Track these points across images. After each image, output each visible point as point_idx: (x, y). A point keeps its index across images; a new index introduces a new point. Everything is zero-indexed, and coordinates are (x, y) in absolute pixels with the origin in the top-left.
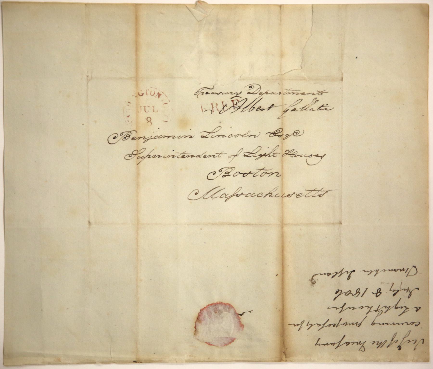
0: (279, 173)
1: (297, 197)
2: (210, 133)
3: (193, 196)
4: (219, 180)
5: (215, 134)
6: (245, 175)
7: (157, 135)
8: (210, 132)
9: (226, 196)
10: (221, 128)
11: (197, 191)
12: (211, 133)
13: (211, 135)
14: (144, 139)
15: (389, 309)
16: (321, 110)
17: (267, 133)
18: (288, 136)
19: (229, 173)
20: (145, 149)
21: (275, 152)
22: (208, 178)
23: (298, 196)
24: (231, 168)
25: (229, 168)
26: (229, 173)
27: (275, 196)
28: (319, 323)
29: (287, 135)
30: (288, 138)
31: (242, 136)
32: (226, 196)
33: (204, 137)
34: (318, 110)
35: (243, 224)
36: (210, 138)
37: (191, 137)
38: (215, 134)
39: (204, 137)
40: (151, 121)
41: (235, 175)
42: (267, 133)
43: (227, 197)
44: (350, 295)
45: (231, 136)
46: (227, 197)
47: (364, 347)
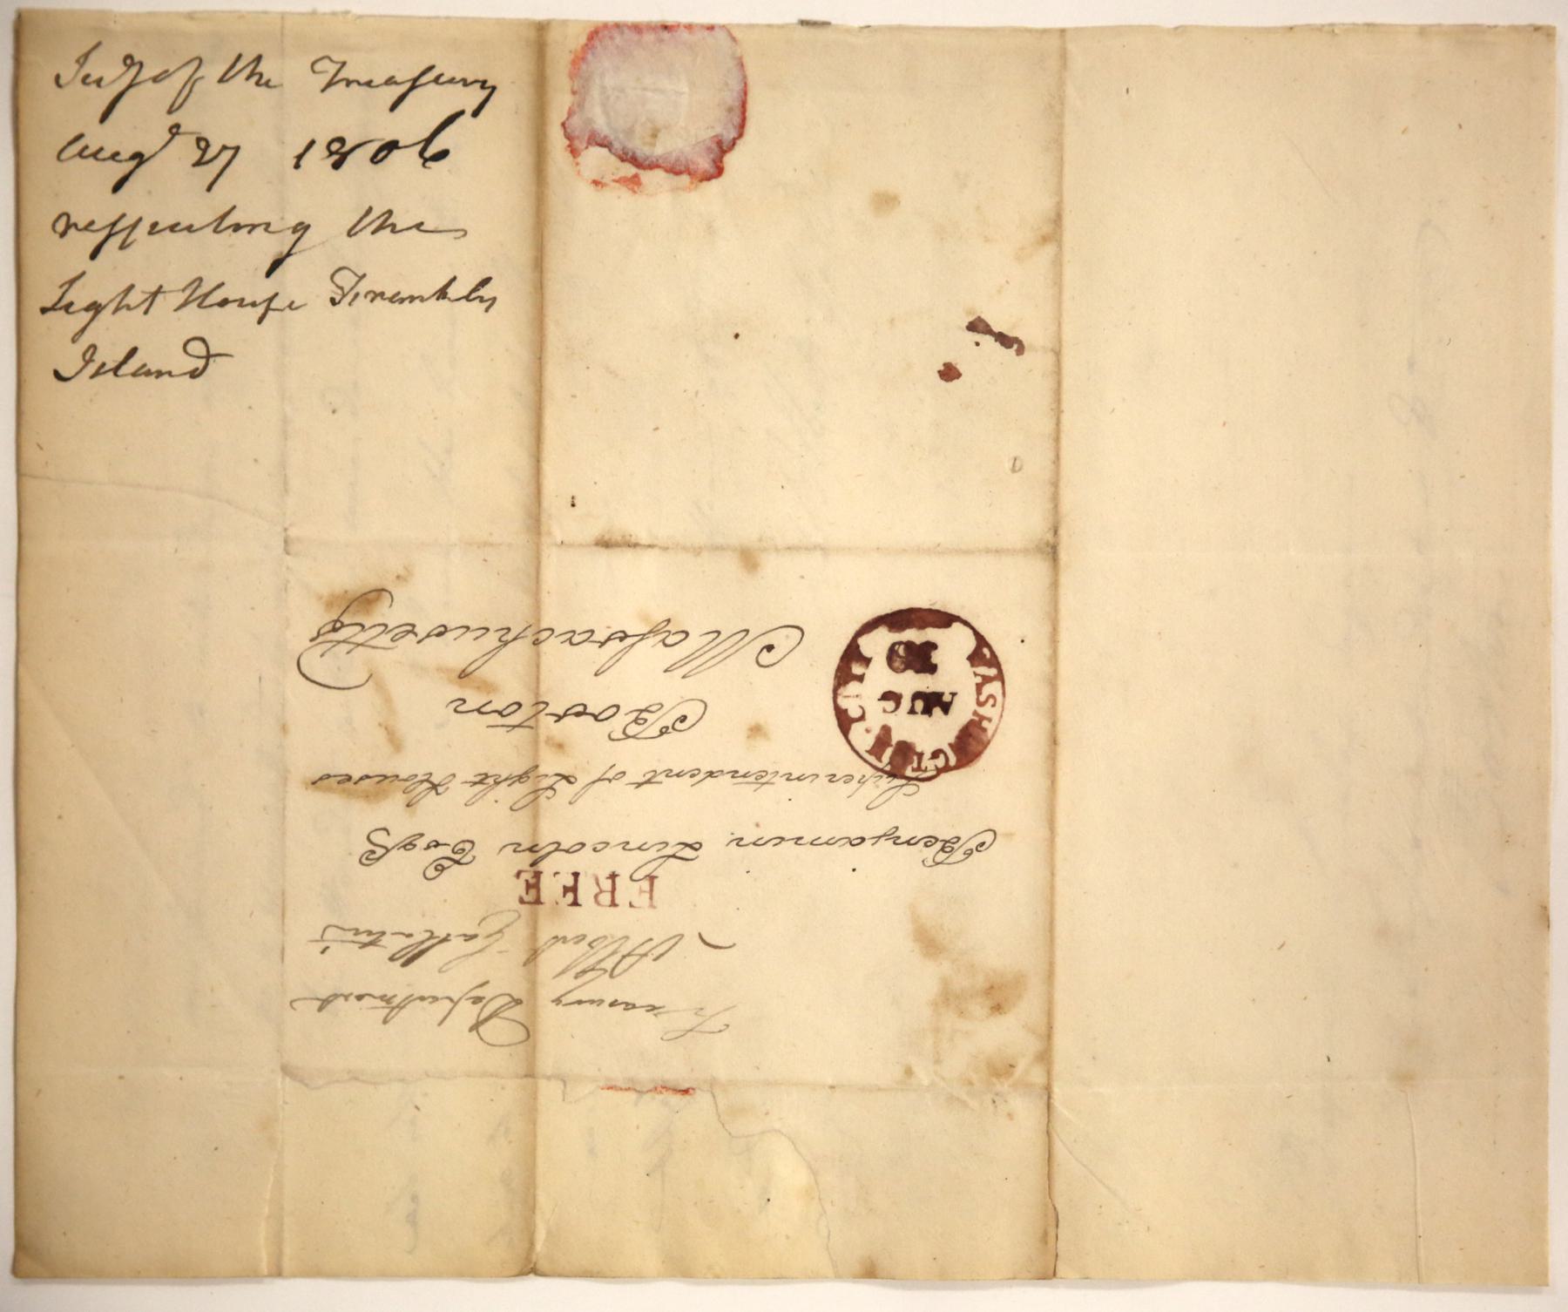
0: (455, 711)
1: (414, 626)
2: (674, 856)
3: (783, 640)
4: (671, 693)
5: (652, 854)
6: (580, 709)
7: (856, 848)
8: (672, 860)
9: (570, 639)
10: (631, 877)
11: (766, 658)
12: (669, 857)
13: (669, 851)
14: (899, 838)
15: (251, 67)
16: (370, 933)
17: (692, 860)
18: (404, 843)
19: (636, 721)
20: (514, 808)
21: (479, 787)
22: (703, 706)
23: (409, 628)
24: (628, 737)
25: (634, 737)
26: (636, 721)
27: (488, 630)
28: (263, 89)
29: (408, 847)
30: (408, 835)
31: (561, 847)
32: (570, 639)
33: (690, 846)
34: (383, 933)
35: (1053, 489)
36: (672, 842)
37: (739, 841)
38: (652, 854)
39: (690, 846)
40: (598, 890)
41: (614, 709)
42: (692, 860)
43: (665, 632)
44: (72, 231)
45: (599, 847)
46: (665, 632)
47: (624, 732)
